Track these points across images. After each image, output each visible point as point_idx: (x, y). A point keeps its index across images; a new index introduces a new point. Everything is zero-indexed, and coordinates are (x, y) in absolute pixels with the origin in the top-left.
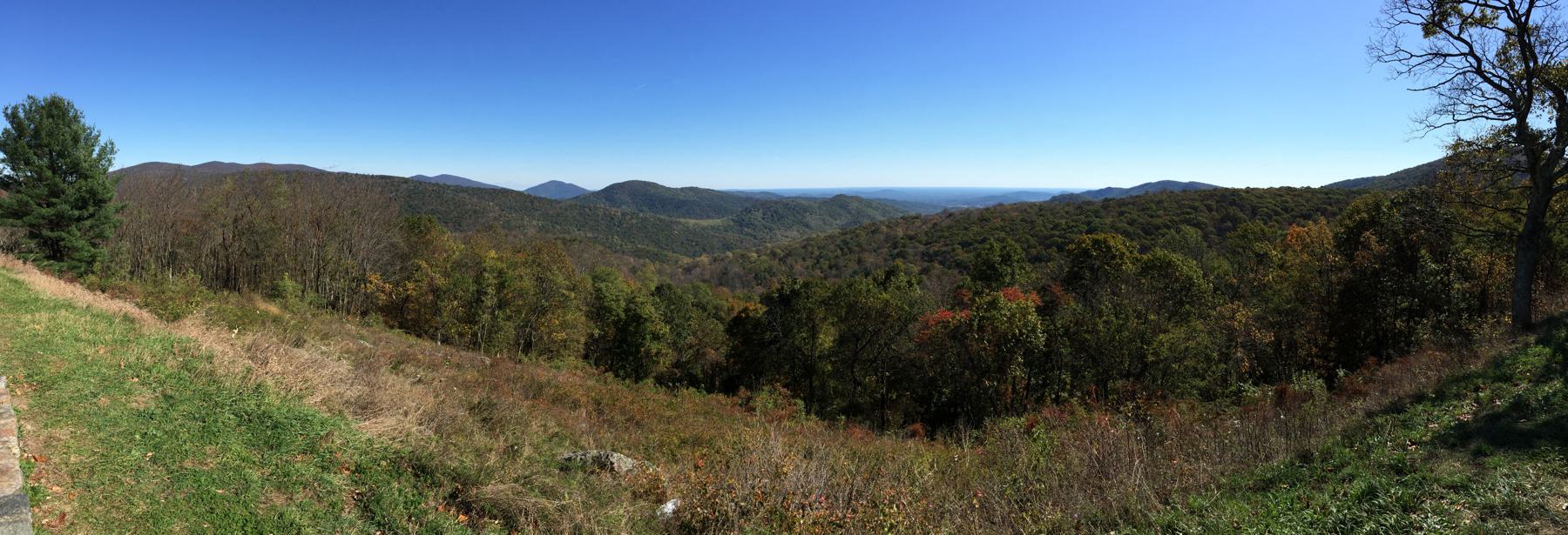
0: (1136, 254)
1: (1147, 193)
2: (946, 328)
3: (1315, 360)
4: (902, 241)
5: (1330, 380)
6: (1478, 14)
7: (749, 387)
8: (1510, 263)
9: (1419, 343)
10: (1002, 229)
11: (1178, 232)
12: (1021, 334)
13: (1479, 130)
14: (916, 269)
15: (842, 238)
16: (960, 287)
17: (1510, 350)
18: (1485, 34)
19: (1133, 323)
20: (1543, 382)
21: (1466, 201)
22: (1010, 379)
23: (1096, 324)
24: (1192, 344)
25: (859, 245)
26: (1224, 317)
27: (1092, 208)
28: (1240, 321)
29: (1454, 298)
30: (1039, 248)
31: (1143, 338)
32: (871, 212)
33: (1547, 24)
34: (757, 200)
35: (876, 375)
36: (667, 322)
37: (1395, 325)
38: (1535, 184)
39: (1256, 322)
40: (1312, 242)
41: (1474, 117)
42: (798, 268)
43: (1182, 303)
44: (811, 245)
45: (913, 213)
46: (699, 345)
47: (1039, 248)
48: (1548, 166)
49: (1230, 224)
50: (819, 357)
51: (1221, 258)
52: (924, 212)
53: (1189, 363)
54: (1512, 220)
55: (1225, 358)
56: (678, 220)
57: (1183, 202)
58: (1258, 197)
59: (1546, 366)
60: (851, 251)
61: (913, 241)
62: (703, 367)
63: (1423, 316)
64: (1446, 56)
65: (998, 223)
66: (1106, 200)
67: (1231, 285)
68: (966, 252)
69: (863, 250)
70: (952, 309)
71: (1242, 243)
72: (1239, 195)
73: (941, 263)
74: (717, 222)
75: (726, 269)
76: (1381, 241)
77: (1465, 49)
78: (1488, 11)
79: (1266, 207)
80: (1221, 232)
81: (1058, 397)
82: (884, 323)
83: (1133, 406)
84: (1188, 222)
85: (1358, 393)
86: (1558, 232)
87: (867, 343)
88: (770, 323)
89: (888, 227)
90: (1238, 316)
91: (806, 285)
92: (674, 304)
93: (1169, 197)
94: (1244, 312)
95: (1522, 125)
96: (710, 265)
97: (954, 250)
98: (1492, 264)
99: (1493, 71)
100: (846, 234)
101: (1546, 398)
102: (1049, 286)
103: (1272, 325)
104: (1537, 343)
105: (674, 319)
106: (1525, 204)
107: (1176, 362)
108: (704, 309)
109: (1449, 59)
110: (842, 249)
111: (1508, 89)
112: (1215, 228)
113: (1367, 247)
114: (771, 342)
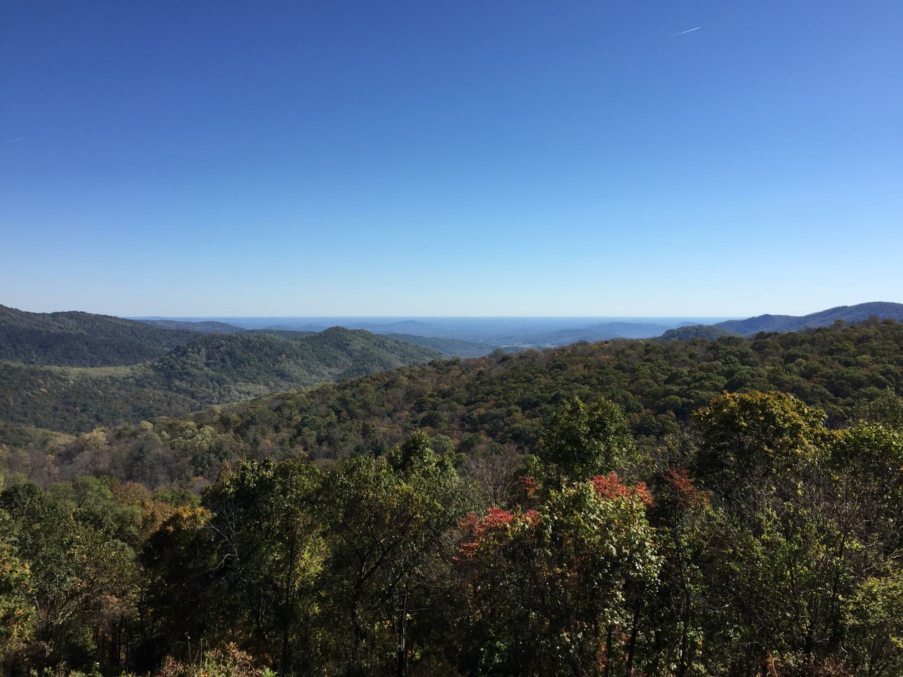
1: (838, 324)
4: (431, 399)
7: (182, 656)
12: (620, 555)
14: (451, 443)
15: (339, 394)
16: (524, 472)
19: (820, 552)
22: (603, 631)
23: (749, 547)
25: (365, 406)
31: (837, 580)
32: (387, 356)
34: (197, 335)
35: (391, 619)
36: (24, 555)
42: (267, 443)
44: (290, 407)
45: (447, 357)
46: (88, 590)
50: (300, 592)
52: (464, 355)
56: (46, 368)
60: (352, 415)
61: (447, 399)
62: (96, 630)
65: (579, 371)
66: (761, 335)
68: (528, 417)
69: (371, 414)
70: (510, 507)
73: (490, 434)
74: (122, 371)
75: (141, 450)
82: (403, 532)
87: (377, 564)
88: (219, 537)
89: (410, 377)
91: (283, 471)
92: (40, 520)
96: (110, 444)
97: (509, 413)
100: (345, 388)
102: (666, 474)
105: (39, 548)
108: (98, 523)
110: (338, 412)
114: (222, 571)
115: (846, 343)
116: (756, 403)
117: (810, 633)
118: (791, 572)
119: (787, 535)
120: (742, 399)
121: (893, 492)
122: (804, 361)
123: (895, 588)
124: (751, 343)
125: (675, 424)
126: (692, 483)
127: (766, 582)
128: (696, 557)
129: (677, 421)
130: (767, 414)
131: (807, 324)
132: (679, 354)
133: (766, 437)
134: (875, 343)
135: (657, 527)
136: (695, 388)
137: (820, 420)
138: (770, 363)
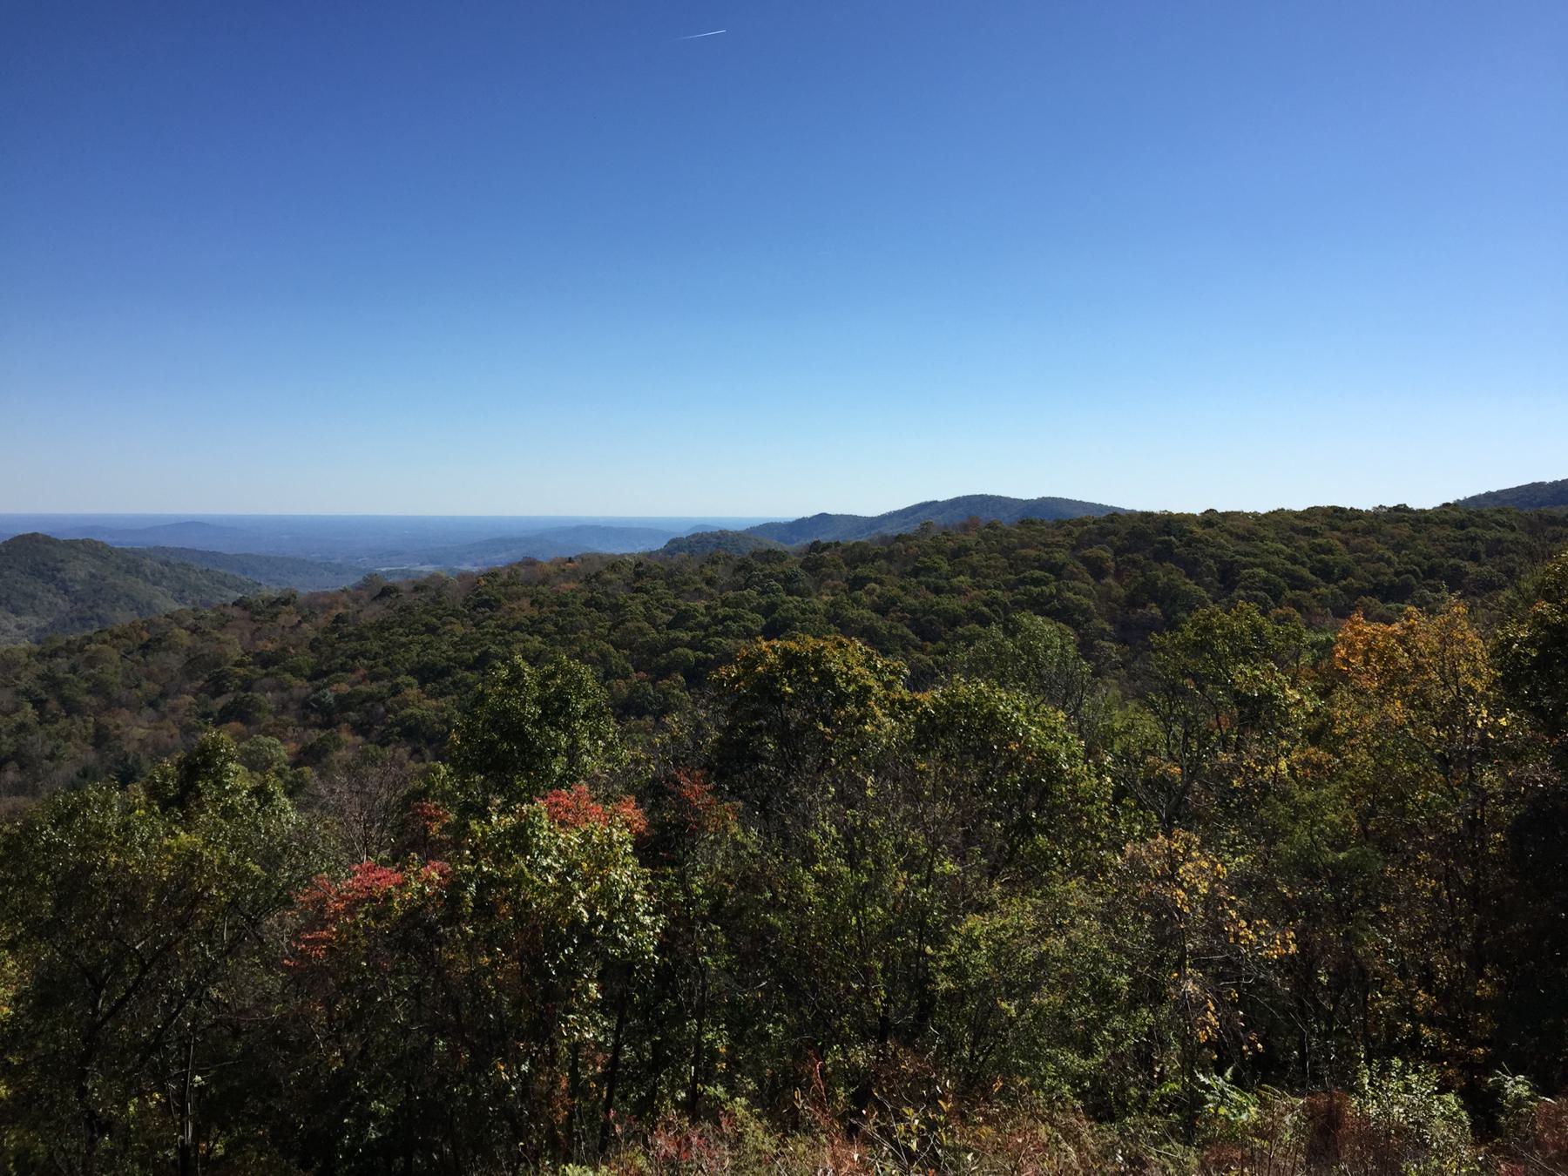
0: (901, 692)
1: (926, 528)
2: (378, 917)
3: (1426, 1032)
4: (241, 671)
10: (534, 627)
11: (1011, 633)
14: (282, 752)
15: (42, 668)
19: (898, 882)
23: (795, 886)
24: (1058, 945)
25: (99, 688)
26: (1144, 873)
28: (1193, 890)
30: (634, 678)
31: (922, 924)
35: (162, 1089)
40: (1418, 668)
43: (1026, 828)
45: (271, 591)
47: (634, 678)
49: (1156, 611)
52: (304, 587)
55: (1150, 992)
57: (1024, 552)
58: (1239, 537)
60: (71, 708)
61: (272, 669)
65: (524, 610)
66: (815, 547)
67: (1164, 783)
68: (431, 695)
70: (395, 860)
71: (1196, 665)
72: (1182, 533)
73: (359, 729)
81: (694, 1096)
82: (182, 925)
84: (1039, 606)
93: (985, 538)
97: (396, 690)
107: (1009, 997)
110: (39, 704)
112: (1112, 621)
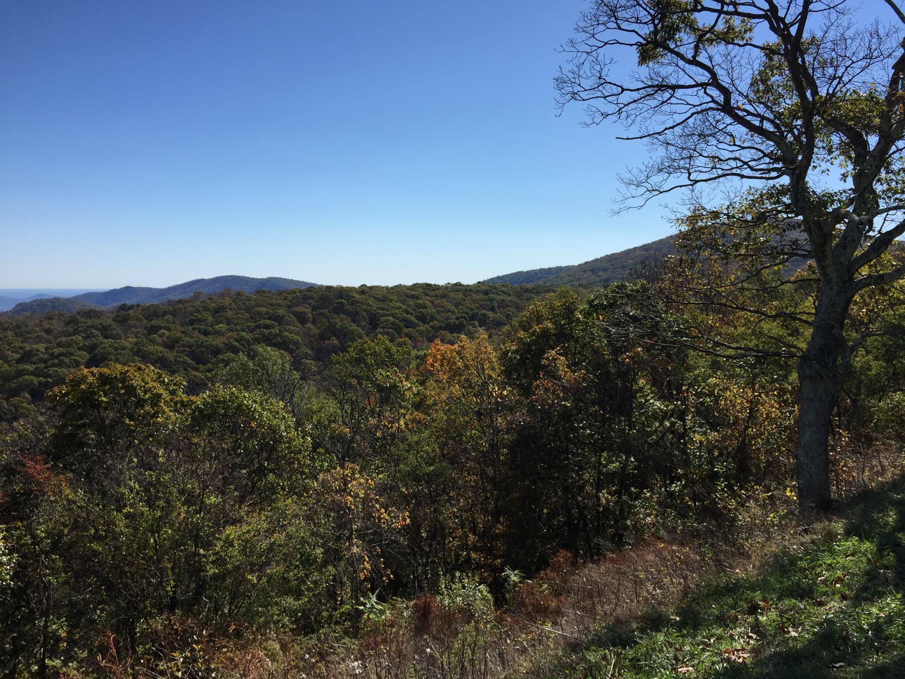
1: (197, 296)
3: (473, 555)
5: (498, 588)
6: (721, 27)
8: (785, 401)
9: (639, 529)
11: (252, 357)
13: (732, 196)
17: (802, 544)
18: (732, 54)
19: (181, 512)
20: (865, 599)
21: (709, 302)
23: (110, 523)
24: (279, 537)
27: (96, 322)
28: (357, 496)
29: (695, 456)
31: (197, 536)
33: (831, 35)
37: (599, 499)
38: (825, 274)
39: (381, 496)
40: (467, 367)
41: (719, 177)
43: (261, 472)
48: (845, 247)
51: (323, 395)
53: (274, 570)
54: (782, 332)
55: (333, 556)
58: (379, 300)
59: (867, 573)
63: (643, 485)
64: (674, 88)
66: (123, 307)
67: (341, 438)
71: (357, 371)
72: (349, 298)
76: (574, 366)
77: (704, 77)
78: (736, 21)
79: (393, 315)
80: (321, 355)
83: (186, 658)
84: (268, 341)
85: (542, 612)
86: (862, 351)
90: (353, 485)
94: (362, 481)
95: (799, 188)
98: (754, 404)
99: (751, 109)
101: (877, 627)
103: (406, 500)
104: (848, 534)
106: (809, 304)
107: (252, 571)
109: (679, 93)
111: (773, 133)
112: (312, 348)
113: (552, 374)
115: (205, 314)
116: (115, 377)
117: (174, 592)
118: (155, 539)
119: (150, 503)
120: (101, 373)
121: (246, 446)
122: (166, 332)
123: (248, 532)
124: (113, 316)
125: (32, 407)
126: (48, 469)
127: (131, 555)
128: (55, 547)
129: (34, 403)
130: (127, 386)
131: (168, 296)
132: (33, 330)
133: (127, 410)
134: (229, 313)
135: (7, 523)
136: (54, 365)
137: (180, 388)
138: (133, 336)
